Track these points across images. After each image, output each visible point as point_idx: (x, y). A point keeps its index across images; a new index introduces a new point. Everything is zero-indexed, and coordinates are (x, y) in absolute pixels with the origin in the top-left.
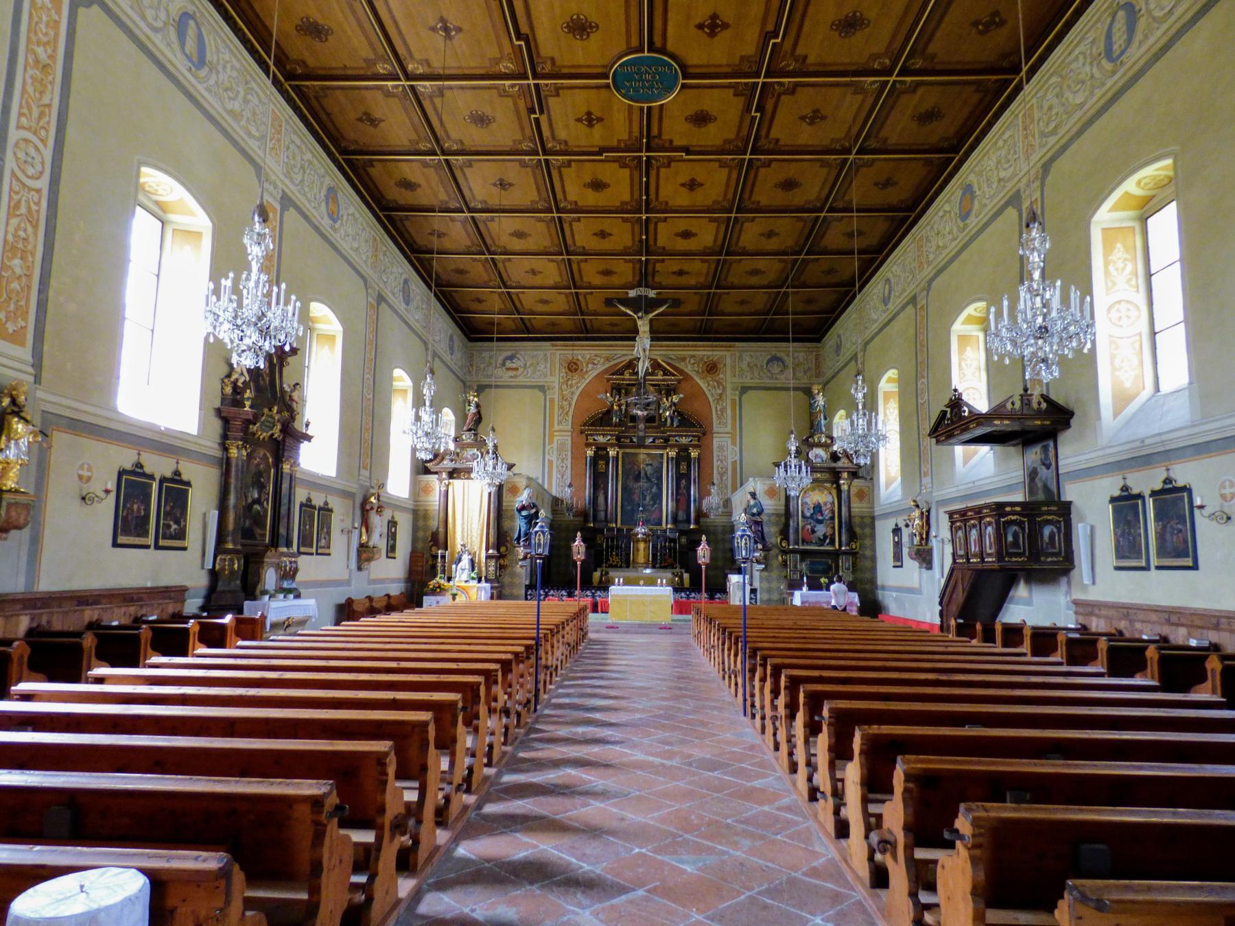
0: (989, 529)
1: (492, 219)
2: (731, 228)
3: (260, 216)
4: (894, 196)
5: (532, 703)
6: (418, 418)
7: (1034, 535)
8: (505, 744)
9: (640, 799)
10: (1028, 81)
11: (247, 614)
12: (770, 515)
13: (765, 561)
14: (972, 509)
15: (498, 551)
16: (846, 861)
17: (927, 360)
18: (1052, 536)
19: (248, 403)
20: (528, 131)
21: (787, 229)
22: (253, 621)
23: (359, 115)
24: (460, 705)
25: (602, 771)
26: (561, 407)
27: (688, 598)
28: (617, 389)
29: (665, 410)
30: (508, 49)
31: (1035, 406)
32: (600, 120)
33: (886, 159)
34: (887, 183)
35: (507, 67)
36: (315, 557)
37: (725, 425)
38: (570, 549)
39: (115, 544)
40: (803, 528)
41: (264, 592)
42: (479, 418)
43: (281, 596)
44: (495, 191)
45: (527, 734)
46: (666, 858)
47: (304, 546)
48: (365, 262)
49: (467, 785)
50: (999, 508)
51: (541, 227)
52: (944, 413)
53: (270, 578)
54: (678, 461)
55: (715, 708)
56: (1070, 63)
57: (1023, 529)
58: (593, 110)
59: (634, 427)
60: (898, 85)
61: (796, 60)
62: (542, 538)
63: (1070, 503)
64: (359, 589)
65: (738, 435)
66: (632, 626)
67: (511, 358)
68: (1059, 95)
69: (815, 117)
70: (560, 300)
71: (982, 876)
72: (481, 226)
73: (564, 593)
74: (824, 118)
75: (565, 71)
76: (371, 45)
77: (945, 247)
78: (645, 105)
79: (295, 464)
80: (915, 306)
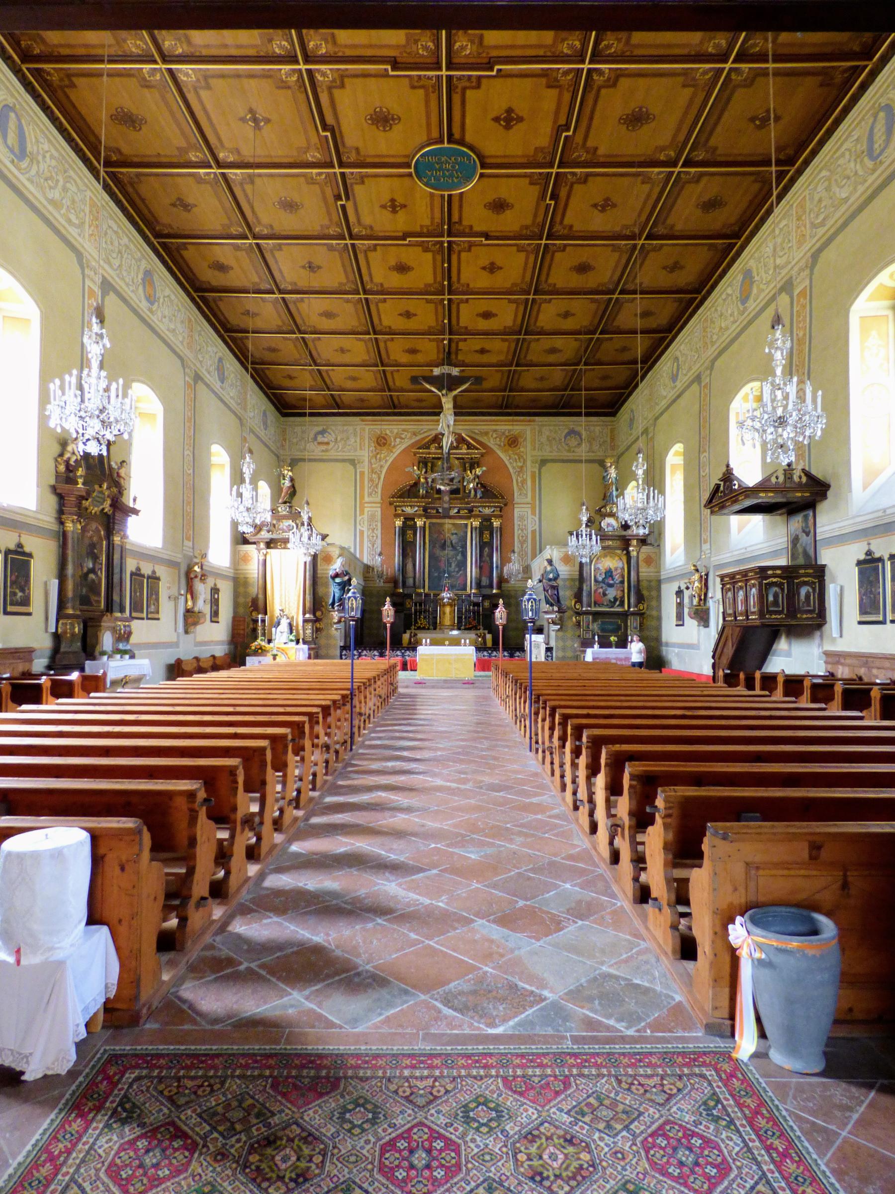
0: (754, 590)
1: (302, 300)
2: (529, 310)
3: (97, 317)
4: (684, 278)
5: (350, 741)
6: (240, 495)
7: (792, 595)
8: (326, 774)
9: (437, 812)
10: (778, 204)
11: (88, 672)
12: (565, 580)
13: (561, 622)
14: (738, 573)
15: (314, 614)
16: (595, 849)
17: (708, 436)
18: (808, 596)
19: (80, 481)
20: (335, 218)
21: (583, 311)
22: (96, 678)
23: (174, 198)
24: (290, 737)
25: (406, 793)
26: (371, 480)
27: (490, 656)
28: (424, 463)
29: (469, 483)
30: (314, 139)
31: (796, 478)
32: (404, 206)
33: (674, 245)
34: (675, 267)
35: (313, 156)
36: (145, 621)
37: (526, 495)
38: (380, 612)
39: (6, 613)
40: (595, 591)
41: (103, 653)
42: (293, 492)
43: (118, 656)
44: (305, 273)
45: (345, 767)
46: (456, 850)
47: (136, 611)
48: (182, 342)
49: (296, 803)
50: (762, 571)
51: (349, 308)
52: (718, 486)
53: (107, 640)
54: (481, 530)
55: (507, 747)
56: (838, 158)
57: (783, 590)
58: (396, 197)
59: (439, 499)
60: (682, 176)
61: (587, 152)
62: (354, 603)
63: (824, 566)
64: (186, 651)
65: (537, 506)
66: (438, 681)
67: (322, 432)
68: (828, 189)
69: (606, 205)
70: (368, 377)
71: (670, 836)
72: (291, 306)
73: (376, 653)
74: (614, 206)
75: (369, 160)
76: (183, 133)
77: (727, 329)
78: (446, 193)
79: (124, 537)
80: (700, 383)
